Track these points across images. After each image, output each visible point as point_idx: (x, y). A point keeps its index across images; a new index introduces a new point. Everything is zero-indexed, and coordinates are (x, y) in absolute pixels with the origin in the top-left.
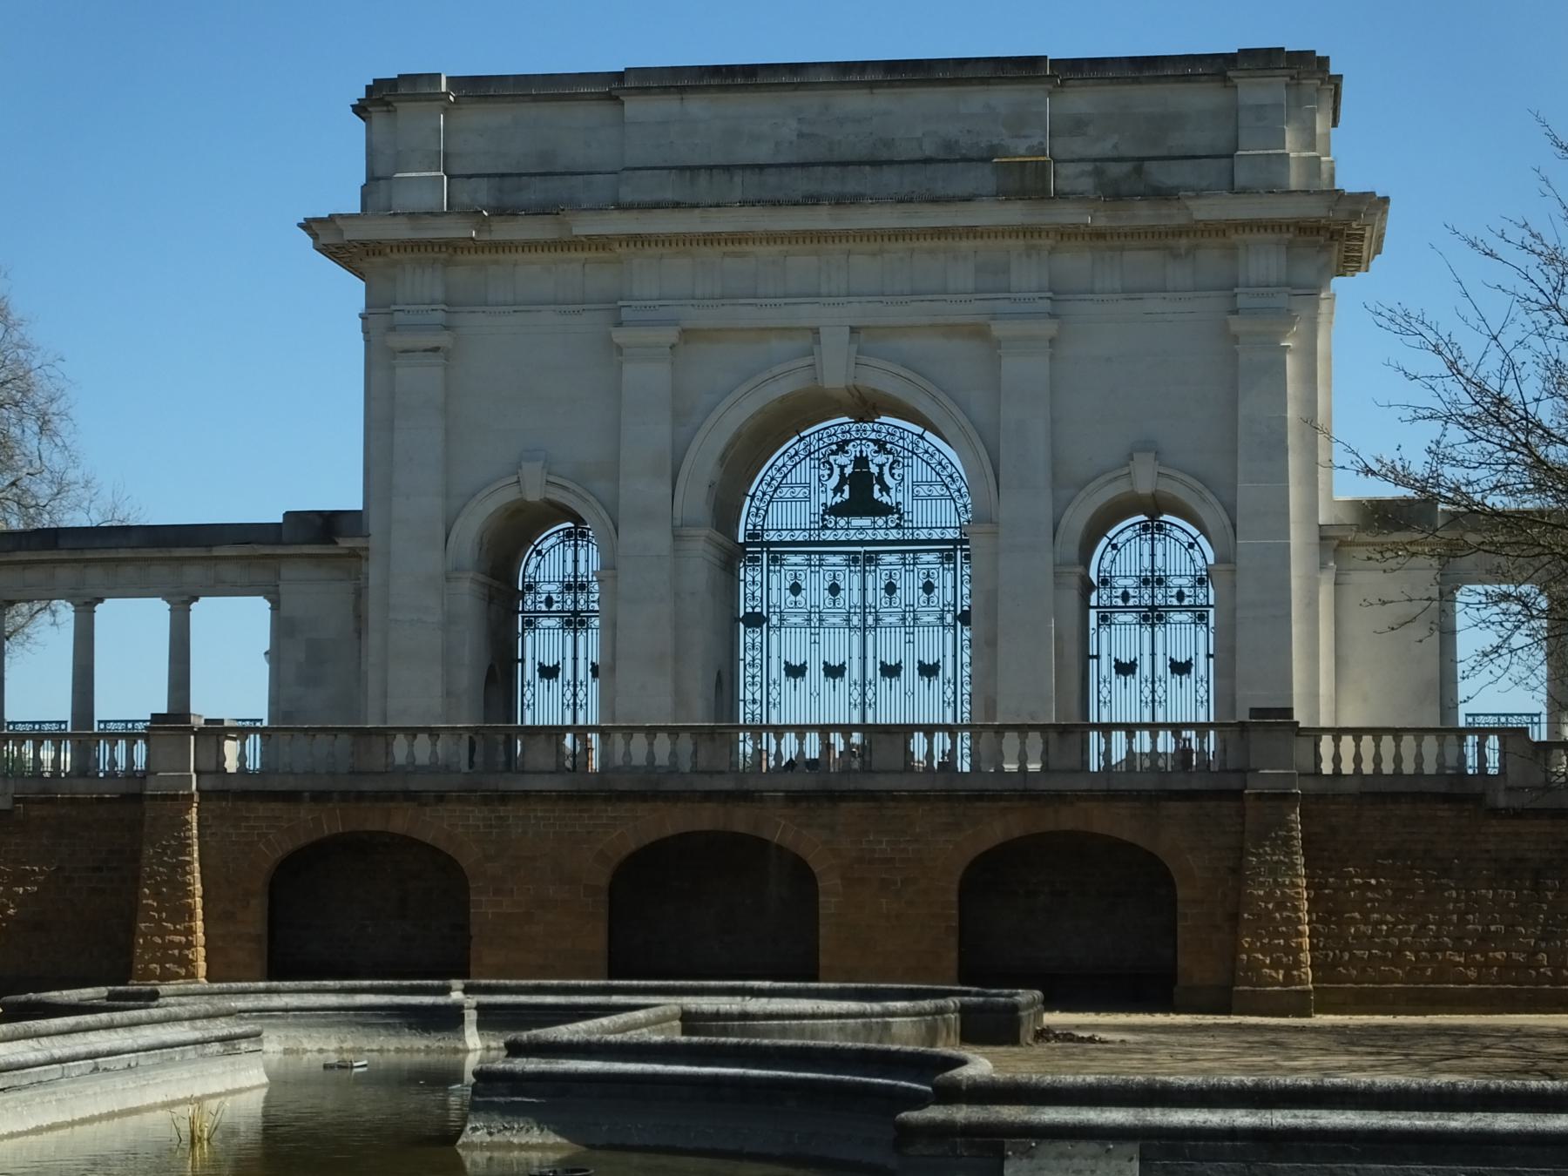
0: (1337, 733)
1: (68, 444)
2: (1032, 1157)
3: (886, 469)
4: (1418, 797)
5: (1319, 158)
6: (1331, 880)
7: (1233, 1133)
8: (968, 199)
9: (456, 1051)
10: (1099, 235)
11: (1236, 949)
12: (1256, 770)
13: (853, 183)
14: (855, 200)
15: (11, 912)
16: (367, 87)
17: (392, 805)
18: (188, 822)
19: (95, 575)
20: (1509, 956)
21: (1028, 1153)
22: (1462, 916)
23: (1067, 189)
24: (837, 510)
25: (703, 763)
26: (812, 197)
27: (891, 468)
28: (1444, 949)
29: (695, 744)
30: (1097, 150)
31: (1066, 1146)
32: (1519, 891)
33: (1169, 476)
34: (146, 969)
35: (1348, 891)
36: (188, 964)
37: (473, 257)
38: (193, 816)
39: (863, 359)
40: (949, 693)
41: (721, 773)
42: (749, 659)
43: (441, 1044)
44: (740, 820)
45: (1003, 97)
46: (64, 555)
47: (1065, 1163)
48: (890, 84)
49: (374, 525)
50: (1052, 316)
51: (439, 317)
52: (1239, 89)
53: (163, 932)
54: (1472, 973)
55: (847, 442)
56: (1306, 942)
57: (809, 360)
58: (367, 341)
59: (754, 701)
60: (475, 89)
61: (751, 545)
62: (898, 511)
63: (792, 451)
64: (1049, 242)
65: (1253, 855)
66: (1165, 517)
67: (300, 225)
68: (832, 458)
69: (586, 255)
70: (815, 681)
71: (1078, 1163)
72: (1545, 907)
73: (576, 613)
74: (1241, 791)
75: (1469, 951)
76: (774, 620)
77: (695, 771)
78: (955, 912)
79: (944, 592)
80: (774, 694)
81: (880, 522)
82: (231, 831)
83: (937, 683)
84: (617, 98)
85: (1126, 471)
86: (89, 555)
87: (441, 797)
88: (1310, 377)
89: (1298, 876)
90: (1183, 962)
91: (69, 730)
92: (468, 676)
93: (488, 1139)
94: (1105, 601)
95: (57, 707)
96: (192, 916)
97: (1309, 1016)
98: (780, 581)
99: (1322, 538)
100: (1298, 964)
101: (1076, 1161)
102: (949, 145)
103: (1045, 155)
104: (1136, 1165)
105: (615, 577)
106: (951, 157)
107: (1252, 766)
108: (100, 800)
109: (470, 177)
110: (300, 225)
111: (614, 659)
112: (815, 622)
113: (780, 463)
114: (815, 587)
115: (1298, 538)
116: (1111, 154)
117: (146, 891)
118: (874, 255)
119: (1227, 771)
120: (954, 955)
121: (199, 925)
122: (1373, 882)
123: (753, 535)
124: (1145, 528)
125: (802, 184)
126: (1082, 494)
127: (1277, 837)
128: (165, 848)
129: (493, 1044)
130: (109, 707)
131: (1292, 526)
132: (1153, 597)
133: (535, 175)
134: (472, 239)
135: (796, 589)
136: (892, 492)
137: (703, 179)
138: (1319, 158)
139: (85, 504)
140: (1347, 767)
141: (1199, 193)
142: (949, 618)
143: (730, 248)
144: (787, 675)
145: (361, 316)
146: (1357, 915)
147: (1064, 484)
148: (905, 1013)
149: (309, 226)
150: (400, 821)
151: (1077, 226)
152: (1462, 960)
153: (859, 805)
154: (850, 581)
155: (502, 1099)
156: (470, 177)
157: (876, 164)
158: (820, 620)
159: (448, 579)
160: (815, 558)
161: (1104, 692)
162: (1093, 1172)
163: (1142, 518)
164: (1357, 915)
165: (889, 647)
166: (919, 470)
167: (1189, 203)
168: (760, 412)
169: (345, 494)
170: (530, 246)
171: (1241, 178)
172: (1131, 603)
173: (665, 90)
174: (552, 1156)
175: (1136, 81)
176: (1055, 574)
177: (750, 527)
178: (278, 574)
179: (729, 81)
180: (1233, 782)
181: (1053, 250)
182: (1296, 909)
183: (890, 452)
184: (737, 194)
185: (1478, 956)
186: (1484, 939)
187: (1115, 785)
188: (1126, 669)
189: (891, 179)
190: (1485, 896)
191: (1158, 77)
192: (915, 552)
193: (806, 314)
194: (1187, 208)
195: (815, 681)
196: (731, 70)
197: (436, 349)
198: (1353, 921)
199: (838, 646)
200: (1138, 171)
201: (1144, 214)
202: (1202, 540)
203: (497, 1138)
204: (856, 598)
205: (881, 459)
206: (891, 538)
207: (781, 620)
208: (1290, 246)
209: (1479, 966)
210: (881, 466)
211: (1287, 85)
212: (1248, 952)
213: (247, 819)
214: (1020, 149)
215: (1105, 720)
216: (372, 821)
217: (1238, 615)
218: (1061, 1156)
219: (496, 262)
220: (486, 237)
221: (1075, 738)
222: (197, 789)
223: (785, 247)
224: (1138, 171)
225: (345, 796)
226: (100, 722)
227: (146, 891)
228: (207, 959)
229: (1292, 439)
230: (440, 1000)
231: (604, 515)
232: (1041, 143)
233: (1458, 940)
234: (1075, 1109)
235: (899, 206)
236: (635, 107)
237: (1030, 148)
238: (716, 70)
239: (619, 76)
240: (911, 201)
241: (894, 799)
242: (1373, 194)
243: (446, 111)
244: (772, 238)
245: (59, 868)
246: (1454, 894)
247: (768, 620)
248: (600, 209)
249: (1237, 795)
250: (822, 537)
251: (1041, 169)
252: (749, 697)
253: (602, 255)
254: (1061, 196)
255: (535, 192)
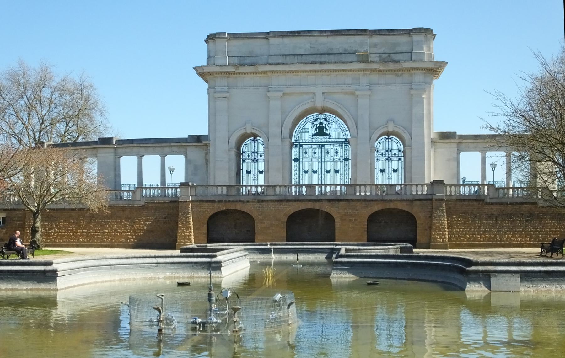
0: (451, 186)
1: (107, 118)
2: (496, 277)
3: (327, 125)
4: (469, 200)
5: (431, 53)
6: (450, 219)
7: (540, 272)
8: (351, 62)
9: (270, 258)
10: (380, 71)
11: (431, 234)
12: (435, 194)
13: (324, 58)
14: (325, 63)
15: (145, 228)
16: (208, 35)
17: (237, 203)
18: (189, 207)
19: (142, 150)
20: (490, 236)
21: (496, 276)
22: (479, 227)
23: (373, 60)
24: (315, 135)
25: (308, 193)
26: (314, 62)
27: (328, 125)
28: (475, 234)
29: (307, 189)
30: (380, 51)
31: (504, 275)
32: (492, 221)
33: (396, 127)
34: (180, 241)
35: (453, 221)
36: (190, 239)
37: (234, 76)
38: (190, 206)
39: (325, 100)
40: (342, 177)
41: (313, 195)
42: (295, 169)
43: (267, 257)
44: (317, 206)
45: (358, 39)
46: (135, 145)
47: (504, 278)
48: (332, 35)
49: (211, 138)
50: (369, 90)
51: (226, 90)
52: (413, 37)
53: (184, 232)
54: (482, 240)
55: (317, 119)
56: (447, 233)
57: (313, 100)
58: (209, 95)
59: (296, 179)
60: (234, 36)
61: (295, 143)
62: (330, 135)
63: (305, 121)
64: (369, 72)
65: (435, 213)
66: (391, 136)
67: (194, 68)
68: (314, 123)
69: (261, 75)
70: (310, 174)
71: (507, 278)
72: (498, 225)
73: (255, 158)
74: (432, 199)
75: (481, 235)
76: (301, 160)
77: (346, 194)
78: (366, 227)
79: (340, 154)
80: (301, 177)
81: (325, 137)
82: (199, 209)
83: (339, 174)
84: (268, 38)
85: (386, 126)
86: (141, 145)
87: (248, 201)
88: (429, 104)
89: (445, 218)
90: (418, 237)
91: (160, 186)
92: (233, 174)
93: (337, 276)
94: (244, 157)
95: (157, 180)
96: (191, 229)
97: (448, 249)
98: (302, 151)
99: (431, 141)
100: (445, 238)
101: (506, 278)
102: (345, 50)
103: (368, 52)
104: (519, 278)
105: (268, 150)
106: (346, 53)
107: (435, 193)
108: (165, 202)
109: (233, 57)
110: (194, 68)
111: (268, 169)
112: (332, 160)
113: (302, 124)
114: (310, 152)
115: (427, 141)
116: (382, 52)
117: (180, 223)
118: (328, 75)
119: (428, 194)
120: (366, 236)
121: (192, 231)
122: (459, 219)
123: (296, 140)
124: (253, 140)
125: (312, 59)
126: (376, 131)
127: (440, 209)
128: (184, 213)
129: (277, 257)
130: (146, 181)
131: (425, 138)
132: (389, 154)
133: (249, 56)
134: (235, 71)
135: (306, 153)
136: (328, 130)
137: (288, 57)
138: (431, 53)
139: (111, 132)
140: (453, 194)
141: (405, 61)
142: (342, 159)
143: (295, 74)
144: (259, 173)
145: (207, 90)
146: (455, 227)
147: (372, 129)
148: (392, 249)
149: (195, 68)
150: (239, 207)
151: (376, 69)
152: (480, 237)
153: (344, 202)
154: (318, 151)
155: (340, 267)
156: (233, 57)
157: (328, 54)
158: (312, 160)
159: (229, 151)
160: (310, 146)
161: (377, 176)
162: (510, 280)
163: (253, 138)
164: (455, 227)
165: (327, 166)
166: (334, 125)
167: (402, 64)
168: (301, 112)
169: (203, 130)
170: (247, 73)
171: (413, 58)
172: (384, 156)
173: (279, 36)
174: (352, 279)
175: (389, 35)
176: (370, 149)
177: (295, 138)
178: (187, 150)
179: (294, 35)
180: (430, 197)
181: (370, 74)
182: (445, 225)
183: (328, 121)
184: (296, 61)
185: (483, 236)
186: (484, 232)
187: (367, 198)
188: (382, 171)
189: (332, 57)
190: (484, 222)
191: (394, 34)
192: (333, 144)
193: (312, 89)
194: (402, 65)
195: (310, 174)
196: (295, 32)
197: (225, 97)
198: (455, 228)
199: (316, 166)
200: (389, 56)
201: (391, 66)
202: (400, 141)
203: (339, 276)
204: (320, 155)
205: (326, 123)
206: (328, 141)
207: (303, 160)
208: (425, 74)
209: (483, 238)
210: (326, 124)
211: (424, 36)
212: (434, 235)
213: (203, 206)
214: (362, 51)
215: (301, 184)
216: (232, 207)
217: (413, 159)
218: (503, 277)
219: (240, 77)
220: (238, 71)
221: (394, 187)
222: (191, 200)
223: (308, 74)
224: (389, 56)
225: (226, 201)
226: (168, 184)
227: (180, 223)
228: (194, 238)
229: (425, 119)
230: (266, 247)
231: (265, 135)
232: (367, 50)
233: (479, 232)
234: (504, 267)
235: (335, 64)
236: (272, 40)
237: (364, 51)
238: (291, 32)
239: (268, 33)
240: (338, 63)
241: (352, 201)
242: (445, 62)
243: (227, 41)
244: (305, 71)
245: (156, 218)
246: (478, 222)
247: (299, 160)
248: (265, 64)
249: (431, 200)
250: (312, 141)
251: (367, 56)
252: (295, 178)
253: (264, 75)
254: (371, 62)
255: (248, 60)
